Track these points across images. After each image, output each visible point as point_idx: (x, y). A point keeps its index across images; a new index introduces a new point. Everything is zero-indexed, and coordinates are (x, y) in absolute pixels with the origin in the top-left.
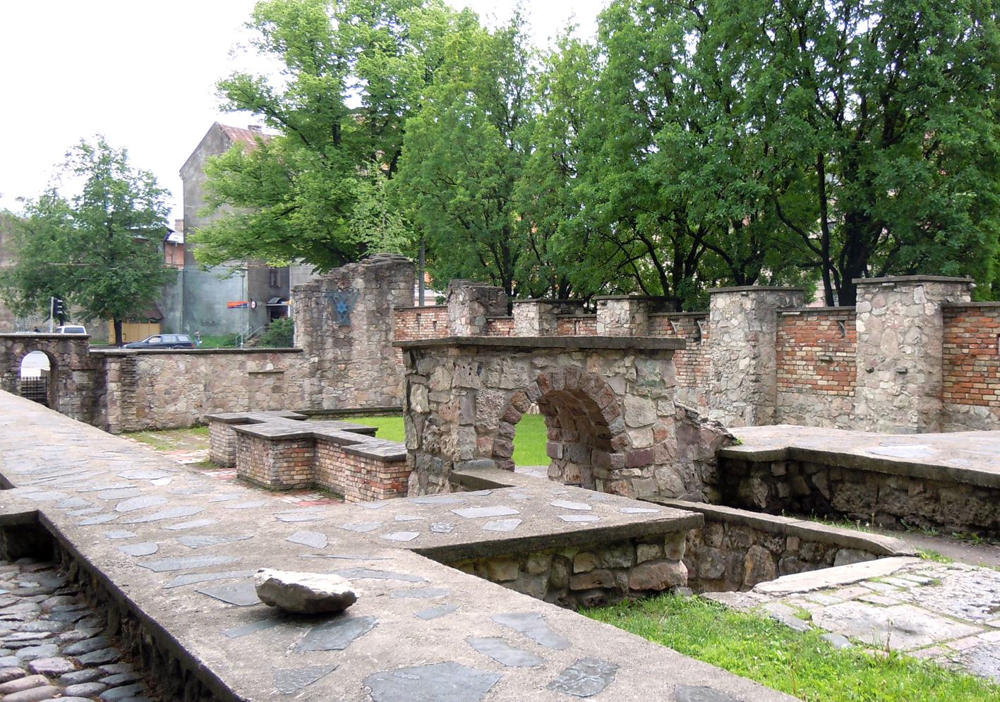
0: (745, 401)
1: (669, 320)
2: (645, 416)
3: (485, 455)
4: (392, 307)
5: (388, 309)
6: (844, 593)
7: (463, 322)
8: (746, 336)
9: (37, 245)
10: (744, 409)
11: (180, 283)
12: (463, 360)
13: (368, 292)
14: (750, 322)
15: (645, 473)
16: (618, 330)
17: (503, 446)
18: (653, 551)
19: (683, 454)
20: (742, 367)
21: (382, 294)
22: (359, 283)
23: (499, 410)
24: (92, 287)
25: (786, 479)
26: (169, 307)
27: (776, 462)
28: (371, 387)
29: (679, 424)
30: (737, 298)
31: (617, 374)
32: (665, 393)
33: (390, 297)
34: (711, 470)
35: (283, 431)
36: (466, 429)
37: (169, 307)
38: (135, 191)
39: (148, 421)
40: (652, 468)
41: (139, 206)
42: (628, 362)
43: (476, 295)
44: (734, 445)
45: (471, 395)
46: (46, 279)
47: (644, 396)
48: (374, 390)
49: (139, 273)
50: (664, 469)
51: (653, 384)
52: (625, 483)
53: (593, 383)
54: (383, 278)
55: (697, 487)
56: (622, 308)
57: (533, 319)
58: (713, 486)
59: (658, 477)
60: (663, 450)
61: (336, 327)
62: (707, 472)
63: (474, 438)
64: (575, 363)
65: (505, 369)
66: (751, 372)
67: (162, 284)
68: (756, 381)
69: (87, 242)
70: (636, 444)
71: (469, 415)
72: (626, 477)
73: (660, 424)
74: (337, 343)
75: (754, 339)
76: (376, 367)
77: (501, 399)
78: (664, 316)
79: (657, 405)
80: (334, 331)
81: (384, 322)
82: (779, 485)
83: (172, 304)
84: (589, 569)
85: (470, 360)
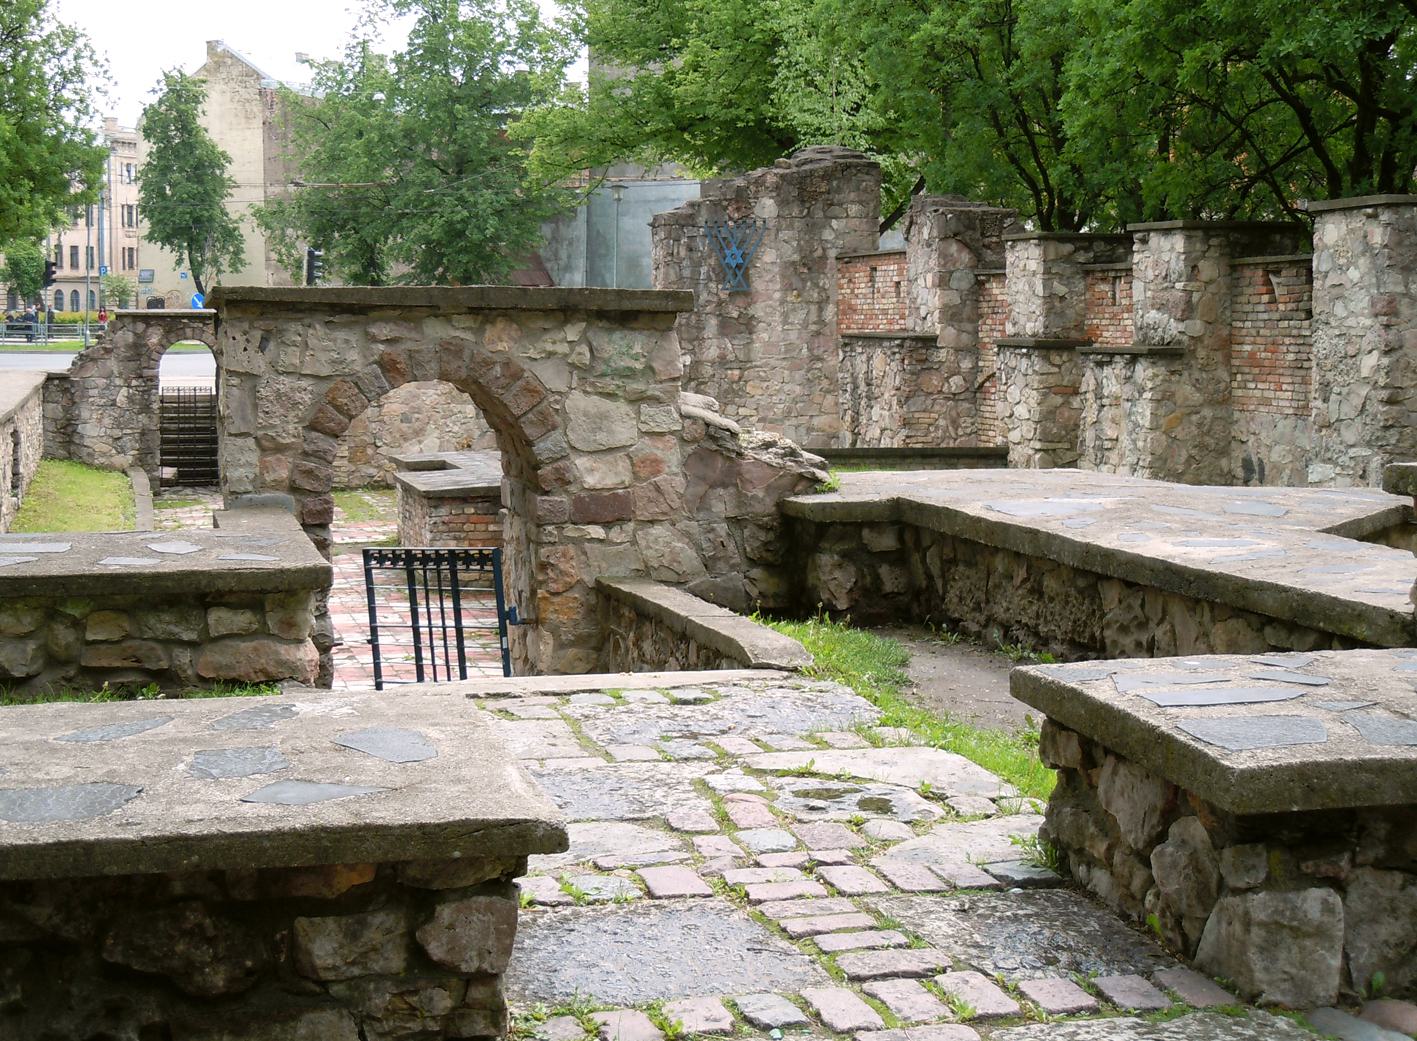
0: (1369, 444)
1: (1267, 273)
2: (610, 432)
3: (276, 485)
4: (832, 253)
5: (824, 257)
6: (491, 704)
7: (929, 284)
8: (1373, 305)
9: (333, 149)
10: (1367, 460)
11: (582, 217)
12: (232, 326)
13: (784, 224)
14: (1379, 272)
15: (615, 534)
16: (1166, 295)
17: (309, 473)
18: (242, 620)
19: (702, 504)
20: (1365, 372)
21: (812, 228)
22: (766, 207)
23: (301, 411)
24: (421, 228)
25: (898, 558)
26: (562, 263)
27: (873, 525)
28: (787, 415)
29: (690, 449)
30: (1358, 221)
31: (551, 355)
32: (654, 390)
33: (828, 235)
34: (762, 536)
35: (457, 483)
36: (240, 441)
37: (562, 263)
38: (499, 39)
39: (372, 471)
40: (632, 525)
41: (508, 68)
42: (572, 332)
43: (953, 226)
44: (816, 492)
45: (248, 385)
46: (347, 212)
47: (611, 396)
48: (794, 421)
49: (503, 199)
50: (657, 530)
51: (630, 374)
52: (572, 550)
53: (498, 370)
54: (815, 196)
55: (733, 567)
56: (1172, 249)
57: (1034, 274)
58: (768, 566)
59: (643, 543)
60: (653, 494)
61: (723, 295)
62: (754, 539)
63: (254, 457)
64: (457, 333)
65: (312, 342)
66: (1382, 382)
67: (544, 219)
68: (1390, 402)
69: (414, 142)
70: (591, 481)
71: (243, 418)
72: (573, 541)
73: (647, 447)
74: (726, 327)
75: (1388, 311)
76: (799, 375)
77: (306, 394)
78: (1257, 265)
79: (638, 413)
80: (720, 303)
81: (816, 285)
82: (884, 570)
83: (569, 257)
84: (116, 637)
85: (246, 326)
